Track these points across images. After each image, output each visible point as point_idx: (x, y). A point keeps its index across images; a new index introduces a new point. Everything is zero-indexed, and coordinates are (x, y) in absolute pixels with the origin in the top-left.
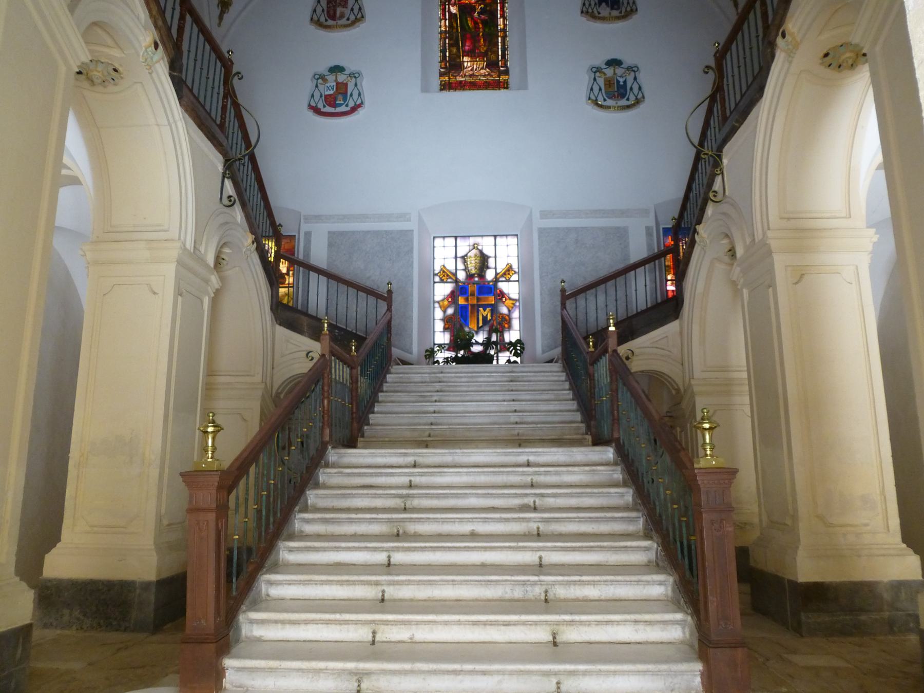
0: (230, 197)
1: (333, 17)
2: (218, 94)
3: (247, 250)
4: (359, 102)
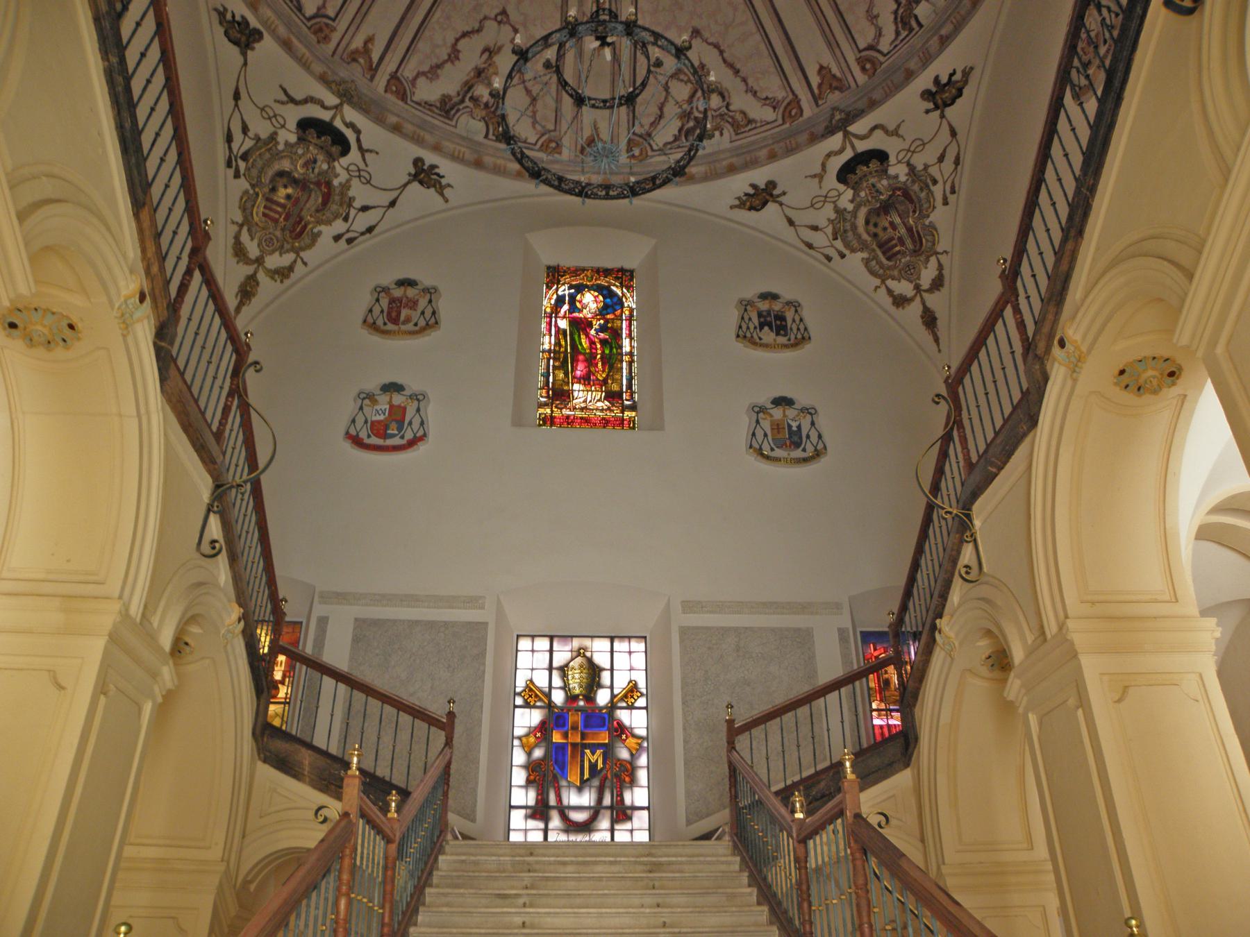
0: (214, 542)
1: (395, 321)
2: (221, 388)
3: (229, 631)
4: (421, 433)
